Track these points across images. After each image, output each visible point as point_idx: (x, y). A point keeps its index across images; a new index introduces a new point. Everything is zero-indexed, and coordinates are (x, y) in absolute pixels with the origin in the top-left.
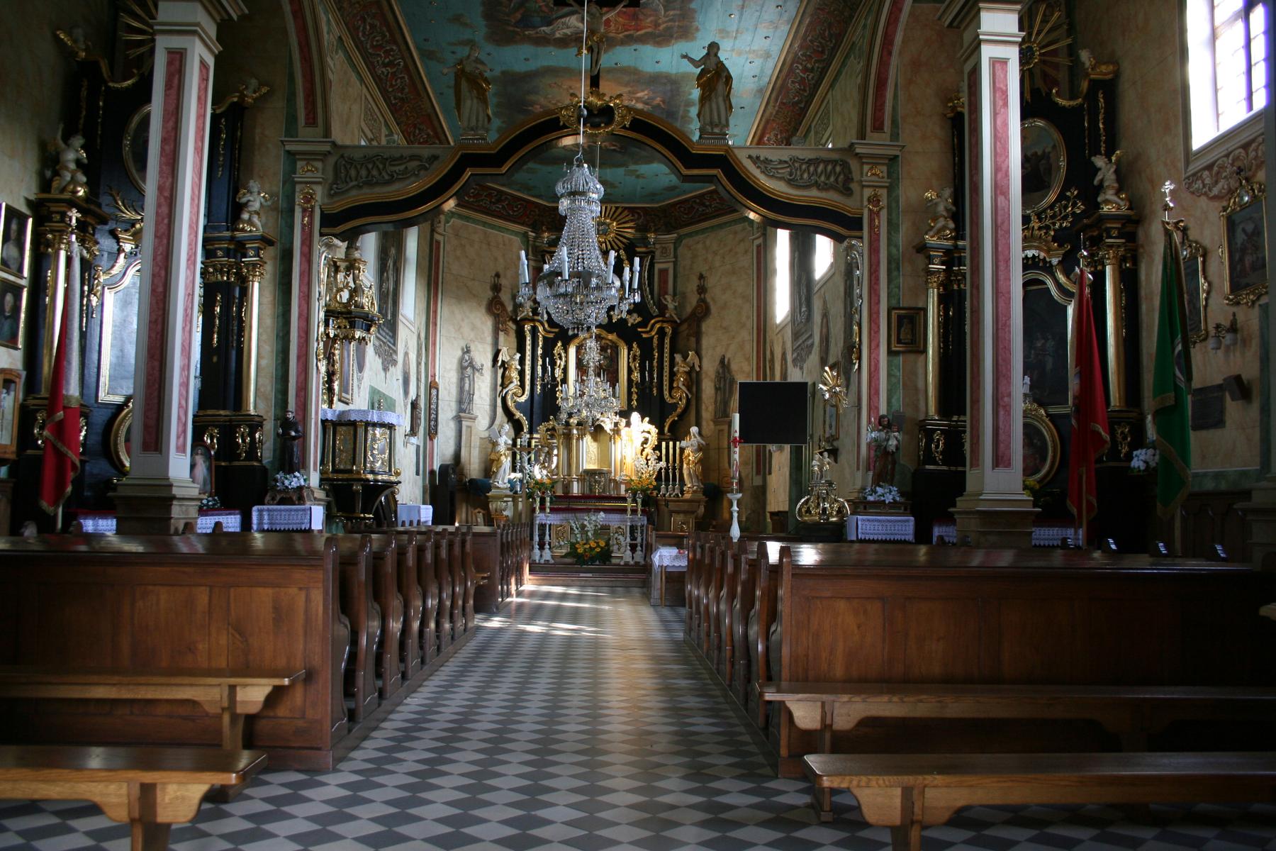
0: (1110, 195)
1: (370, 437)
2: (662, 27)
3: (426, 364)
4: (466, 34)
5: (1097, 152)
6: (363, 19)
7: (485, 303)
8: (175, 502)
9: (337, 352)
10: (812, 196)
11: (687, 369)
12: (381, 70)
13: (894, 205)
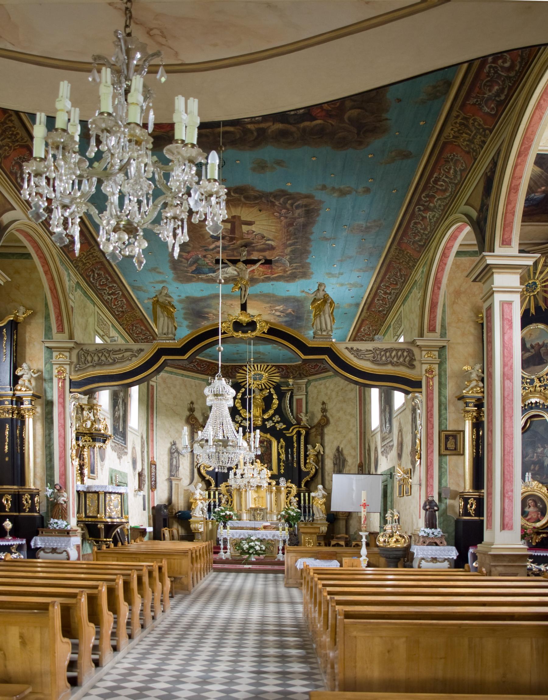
1: (108, 499)
2: (288, 273)
3: (148, 452)
4: (160, 278)
6: (93, 272)
7: (184, 418)
10: (389, 370)
11: (316, 453)
13: (443, 373)
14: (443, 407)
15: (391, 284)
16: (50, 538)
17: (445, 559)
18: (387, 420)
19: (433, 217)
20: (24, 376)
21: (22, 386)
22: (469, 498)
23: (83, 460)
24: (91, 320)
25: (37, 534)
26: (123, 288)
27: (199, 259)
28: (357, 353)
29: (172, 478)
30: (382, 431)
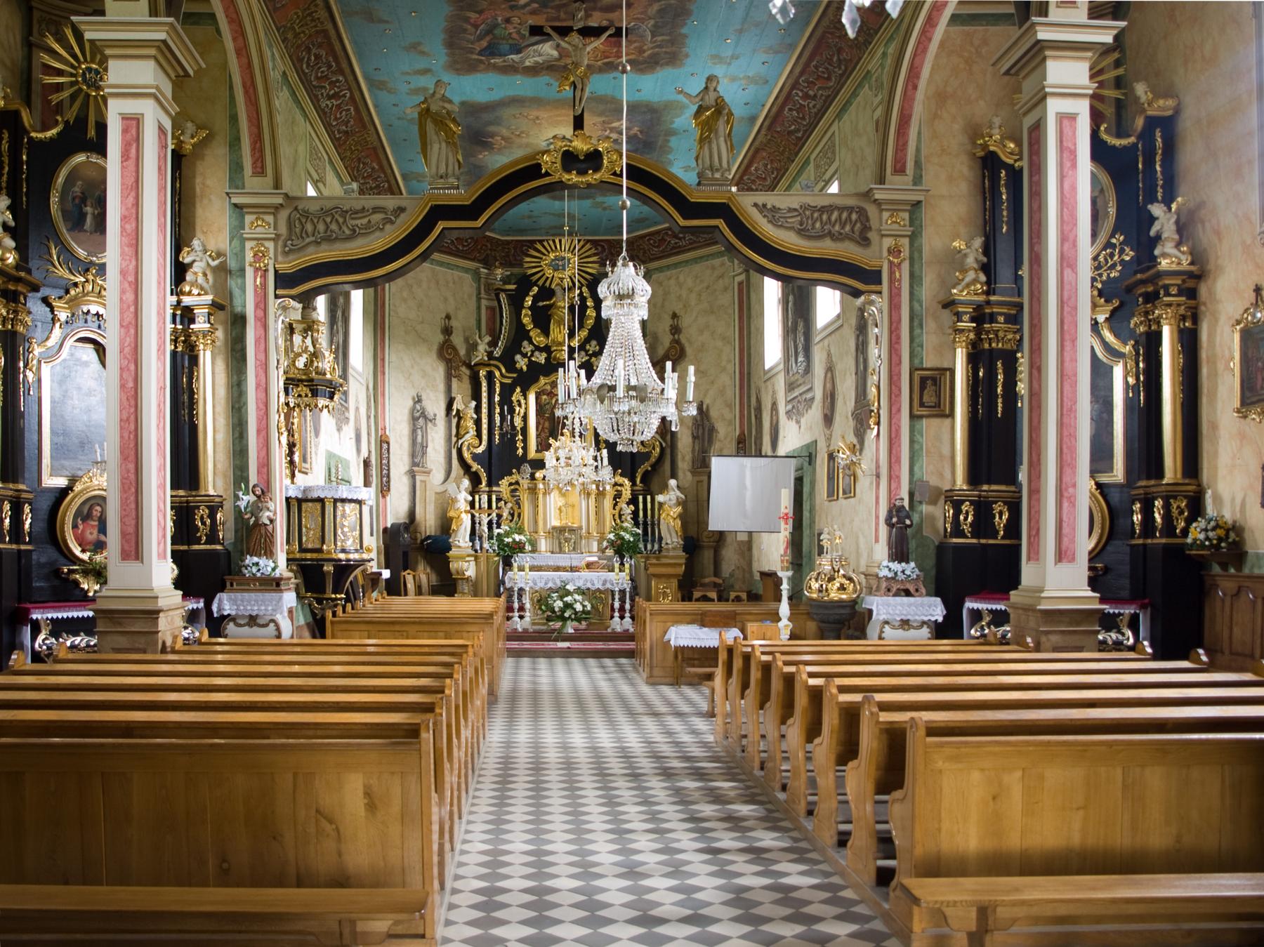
0: (1169, 248)
1: (339, 513)
2: (646, 54)
3: (376, 417)
4: (421, 64)
5: (1153, 200)
6: (309, 50)
7: (435, 347)
8: (161, 615)
9: (296, 421)
10: (826, 248)
12: (324, 103)
13: (916, 255)
14: (916, 323)
15: (819, 77)
16: (246, 595)
17: (924, 623)
20: (195, 264)
21: (192, 285)
22: (963, 502)
24: (301, 148)
25: (222, 589)
26: (354, 85)
27: (496, 26)
28: (772, 214)
29: (416, 469)
30: (787, 370)
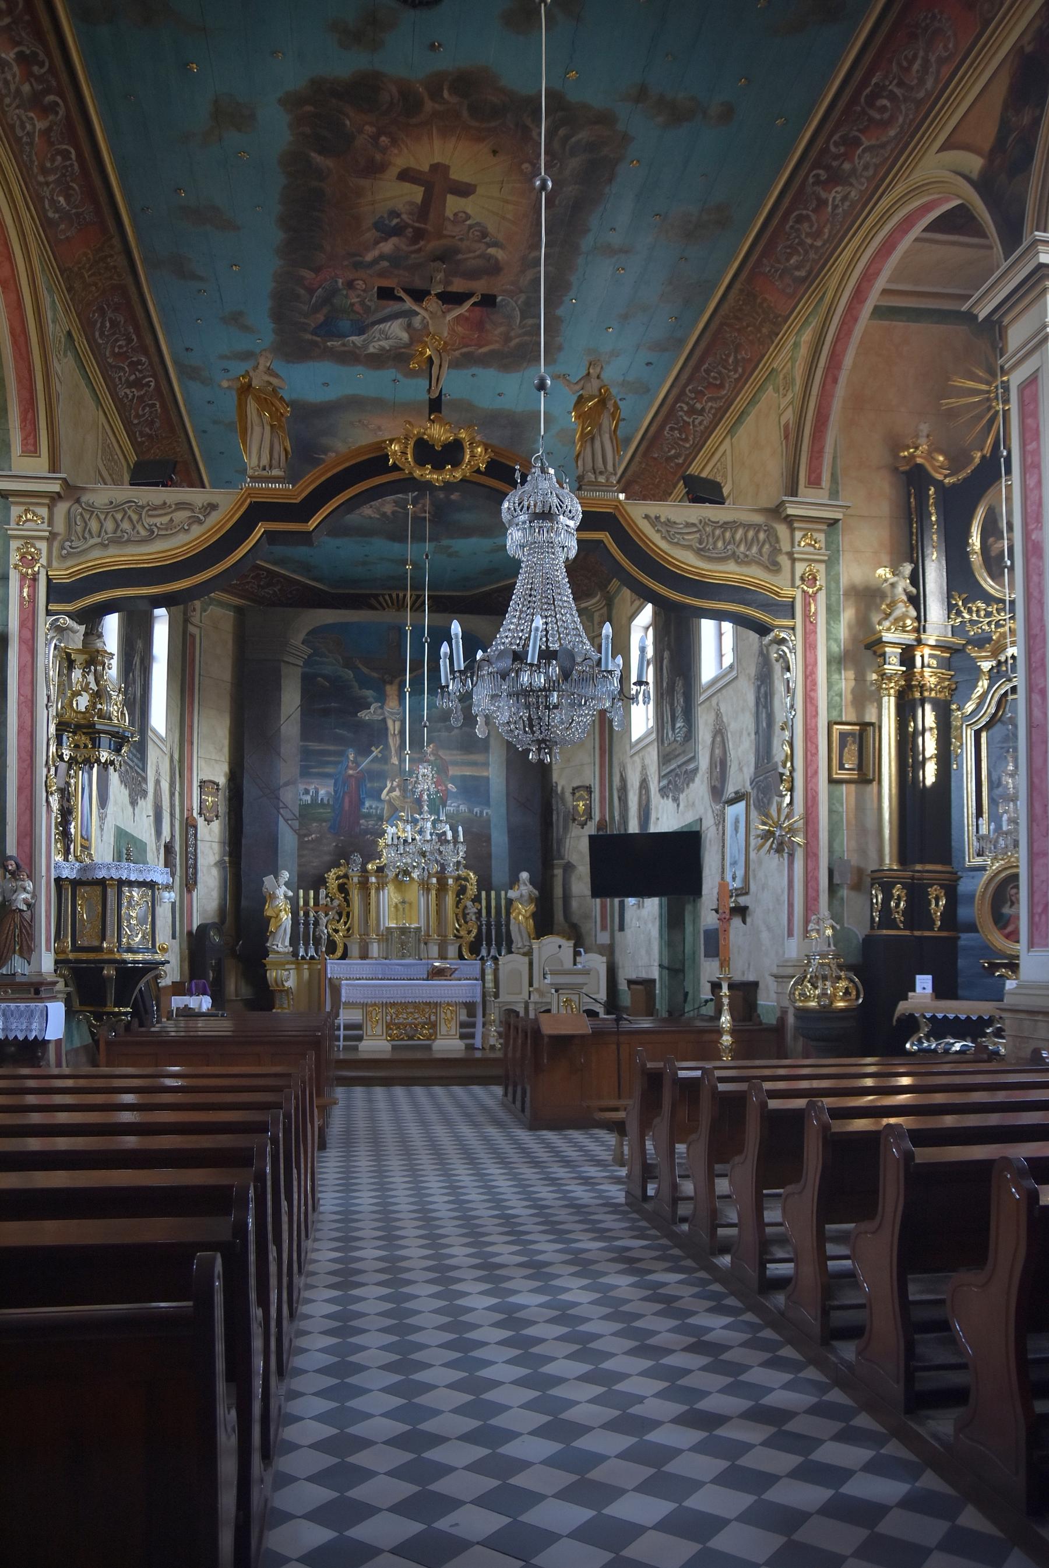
2: (513, 344)
3: (181, 795)
12: (123, 391)
13: (833, 585)
18: (679, 711)
19: (844, 198)
22: (894, 884)
23: (68, 801)
27: (334, 292)
30: (661, 739)
